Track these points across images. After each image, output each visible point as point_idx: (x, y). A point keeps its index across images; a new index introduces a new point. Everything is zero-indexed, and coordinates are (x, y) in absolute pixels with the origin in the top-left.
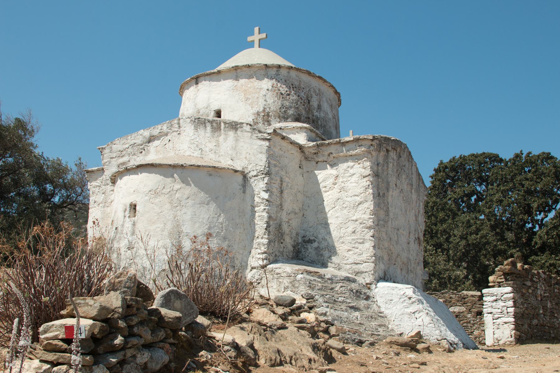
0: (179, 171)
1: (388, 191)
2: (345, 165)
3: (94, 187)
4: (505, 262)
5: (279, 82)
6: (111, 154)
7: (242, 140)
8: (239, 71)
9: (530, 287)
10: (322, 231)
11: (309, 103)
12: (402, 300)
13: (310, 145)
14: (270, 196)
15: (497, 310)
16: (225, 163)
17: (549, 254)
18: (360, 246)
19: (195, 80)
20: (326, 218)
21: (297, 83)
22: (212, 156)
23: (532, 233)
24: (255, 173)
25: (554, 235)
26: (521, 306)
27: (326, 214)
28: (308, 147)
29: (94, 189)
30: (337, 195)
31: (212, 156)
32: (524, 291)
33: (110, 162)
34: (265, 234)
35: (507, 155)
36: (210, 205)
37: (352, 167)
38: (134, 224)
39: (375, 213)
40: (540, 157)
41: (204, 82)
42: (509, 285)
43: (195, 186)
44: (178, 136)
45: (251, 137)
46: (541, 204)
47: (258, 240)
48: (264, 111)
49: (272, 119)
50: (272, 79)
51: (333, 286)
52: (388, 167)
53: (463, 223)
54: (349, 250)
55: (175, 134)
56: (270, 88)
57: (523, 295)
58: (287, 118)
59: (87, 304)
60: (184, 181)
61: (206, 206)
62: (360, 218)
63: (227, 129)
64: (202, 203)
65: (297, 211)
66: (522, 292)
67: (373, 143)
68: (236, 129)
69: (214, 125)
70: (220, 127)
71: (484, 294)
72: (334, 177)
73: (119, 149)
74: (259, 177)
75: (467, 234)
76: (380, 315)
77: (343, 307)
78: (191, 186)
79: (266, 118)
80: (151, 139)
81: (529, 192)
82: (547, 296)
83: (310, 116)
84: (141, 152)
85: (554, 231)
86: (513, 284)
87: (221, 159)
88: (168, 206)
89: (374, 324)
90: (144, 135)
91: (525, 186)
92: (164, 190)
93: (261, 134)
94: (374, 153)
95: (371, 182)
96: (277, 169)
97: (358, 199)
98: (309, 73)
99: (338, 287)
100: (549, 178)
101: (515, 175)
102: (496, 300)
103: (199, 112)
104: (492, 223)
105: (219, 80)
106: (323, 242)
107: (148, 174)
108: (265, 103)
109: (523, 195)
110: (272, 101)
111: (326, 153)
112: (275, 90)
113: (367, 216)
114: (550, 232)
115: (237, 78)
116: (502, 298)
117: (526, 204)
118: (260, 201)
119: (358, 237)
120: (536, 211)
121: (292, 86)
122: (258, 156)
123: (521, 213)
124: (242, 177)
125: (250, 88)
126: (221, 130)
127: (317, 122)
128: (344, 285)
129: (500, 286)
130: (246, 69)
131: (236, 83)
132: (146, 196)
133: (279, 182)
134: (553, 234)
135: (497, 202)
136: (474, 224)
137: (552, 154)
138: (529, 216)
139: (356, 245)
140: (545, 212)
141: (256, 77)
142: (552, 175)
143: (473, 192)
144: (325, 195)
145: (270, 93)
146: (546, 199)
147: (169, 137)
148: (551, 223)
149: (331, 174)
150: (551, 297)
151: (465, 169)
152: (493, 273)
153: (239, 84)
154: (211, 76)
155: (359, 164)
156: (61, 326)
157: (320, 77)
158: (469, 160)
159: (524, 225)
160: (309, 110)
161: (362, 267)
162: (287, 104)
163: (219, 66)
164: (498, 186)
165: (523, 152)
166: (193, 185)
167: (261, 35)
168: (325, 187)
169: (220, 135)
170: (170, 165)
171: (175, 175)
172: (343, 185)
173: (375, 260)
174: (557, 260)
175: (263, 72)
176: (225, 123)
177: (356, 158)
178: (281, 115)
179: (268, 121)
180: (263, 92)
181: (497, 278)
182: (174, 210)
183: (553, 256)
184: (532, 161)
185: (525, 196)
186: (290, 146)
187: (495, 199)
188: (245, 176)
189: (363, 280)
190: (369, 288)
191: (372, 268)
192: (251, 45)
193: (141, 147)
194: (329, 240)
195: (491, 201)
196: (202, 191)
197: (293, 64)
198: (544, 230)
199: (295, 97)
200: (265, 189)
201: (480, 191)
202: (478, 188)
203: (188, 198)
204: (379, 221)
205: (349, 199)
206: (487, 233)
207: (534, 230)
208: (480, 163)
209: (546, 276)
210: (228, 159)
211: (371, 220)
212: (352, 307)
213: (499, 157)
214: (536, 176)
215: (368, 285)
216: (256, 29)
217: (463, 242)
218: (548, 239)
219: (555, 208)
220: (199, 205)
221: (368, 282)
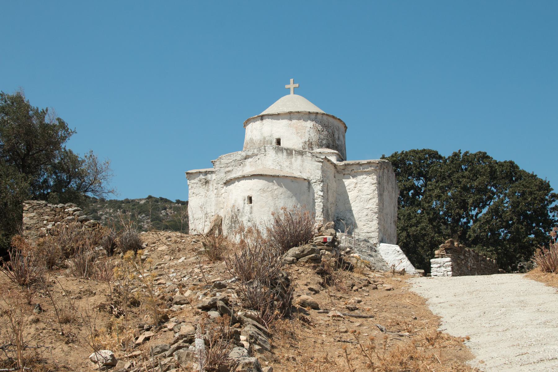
0: (276, 179)
1: (384, 192)
2: (361, 177)
3: (193, 184)
4: (446, 242)
5: (317, 123)
6: (220, 165)
7: (306, 161)
8: (292, 114)
9: (463, 260)
10: (348, 214)
11: (334, 136)
12: (394, 252)
13: (341, 165)
14: (323, 194)
15: (440, 273)
16: (297, 174)
17: (481, 246)
18: (371, 223)
19: (260, 117)
20: (350, 207)
21: (327, 124)
22: (288, 169)
23: (466, 227)
24: (315, 181)
25: (487, 228)
26: (457, 272)
27: (350, 204)
28: (340, 165)
29: (193, 185)
30: (357, 194)
31: (288, 169)
32: (459, 262)
33: (220, 170)
34: (321, 215)
35: (446, 153)
36: (293, 198)
37: (366, 178)
38: (251, 208)
39: (378, 205)
40: (477, 156)
41: (267, 119)
42: (449, 257)
43: (285, 187)
44: (264, 156)
45: (311, 160)
46: (476, 200)
47: (317, 218)
48: (309, 141)
49: (314, 147)
50: (313, 121)
51: (359, 243)
52: (384, 178)
53: (404, 216)
54: (364, 225)
55: (262, 155)
56: (312, 126)
57: (458, 264)
58: (322, 146)
59: (326, 232)
60: (279, 184)
61: (291, 199)
62: (371, 208)
63: (296, 155)
64: (289, 197)
65: (334, 202)
66: (457, 262)
67: (378, 165)
68: (302, 155)
69: (288, 151)
70: (292, 153)
71: (432, 262)
72: (354, 184)
73: (226, 162)
74: (317, 183)
75: (407, 226)
76: (382, 260)
77: (366, 254)
78: (283, 187)
79: (310, 145)
80: (247, 158)
81: (465, 189)
82: (475, 268)
83: (335, 144)
84: (240, 165)
85: (486, 225)
86: (452, 256)
87: (294, 172)
88: (271, 198)
89: (380, 264)
90: (242, 155)
91: (462, 183)
92: (268, 190)
93: (317, 159)
94: (378, 171)
95: (377, 187)
96: (325, 178)
97: (369, 197)
98: (333, 117)
99: (362, 244)
100: (485, 177)
101: (454, 172)
102: (440, 267)
103: (265, 139)
104: (431, 216)
105: (279, 120)
106: (349, 220)
107: (258, 180)
108: (309, 136)
109: (460, 191)
110: (314, 135)
111: (350, 170)
112: (315, 128)
113: (374, 206)
114: (483, 226)
115: (290, 119)
116: (444, 265)
117: (462, 200)
118: (318, 196)
119: (369, 218)
120: (471, 206)
121: (321, 123)
122: (316, 171)
123: (457, 208)
124: (308, 183)
125: (300, 126)
126: (292, 155)
127: (338, 148)
128: (364, 243)
129: (442, 257)
130: (297, 114)
131: (290, 122)
132: (258, 192)
133: (326, 186)
134: (485, 228)
135: (436, 197)
136: (415, 217)
137: (488, 154)
138: (465, 211)
139: (368, 222)
140: (479, 207)
141: (303, 119)
142: (487, 174)
143: (413, 187)
144: (349, 194)
145: (312, 130)
146: (480, 195)
147: (258, 157)
148: (484, 218)
149: (352, 182)
150: (478, 269)
151: (405, 164)
152: (437, 248)
153: (292, 123)
154: (273, 116)
155: (370, 176)
156: (322, 238)
157: (339, 119)
158: (410, 155)
159: (459, 220)
160: (334, 141)
161: (371, 235)
162: (322, 137)
164: (437, 182)
165: (461, 152)
166: (284, 187)
167: (295, 85)
168: (349, 189)
169: (292, 158)
170: (271, 175)
171: (274, 181)
172: (360, 188)
173: (379, 231)
174: (488, 251)
175: (307, 116)
176: (295, 151)
177: (368, 173)
178: (319, 144)
179: (312, 148)
180: (308, 129)
181: (441, 252)
182: (274, 200)
183: (485, 248)
184: (469, 159)
185: (462, 192)
186: (331, 165)
187: (434, 195)
188: (309, 182)
189: (374, 241)
190: (376, 246)
191: (377, 235)
192: (287, 92)
193: (240, 162)
194: (353, 219)
195: (430, 196)
196: (289, 190)
197: (324, 111)
198: (478, 224)
199: (326, 133)
200: (321, 190)
201: (418, 186)
202: (416, 183)
203: (281, 194)
204: (380, 209)
205: (364, 196)
206: (426, 226)
207: (469, 225)
208: (420, 159)
209: (475, 254)
210: (298, 172)
211: (377, 209)
212: (369, 255)
213: (438, 154)
214: (472, 174)
215: (375, 245)
216: (292, 80)
217: (404, 234)
218: (480, 233)
219: (489, 204)
220: (287, 198)
221: (375, 243)
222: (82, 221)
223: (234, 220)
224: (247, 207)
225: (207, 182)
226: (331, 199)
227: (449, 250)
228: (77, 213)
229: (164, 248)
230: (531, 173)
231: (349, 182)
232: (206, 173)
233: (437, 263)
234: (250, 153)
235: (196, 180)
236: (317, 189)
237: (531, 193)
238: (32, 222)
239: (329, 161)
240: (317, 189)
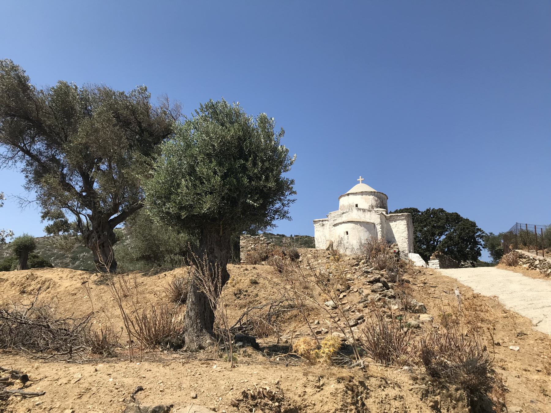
2: (399, 221)
22: (363, 218)
31: (363, 218)
57: (442, 263)
60: (361, 226)
79: (372, 207)
81: (434, 227)
97: (403, 231)
98: (382, 193)
115: (362, 195)
121: (377, 196)
137: (444, 209)
140: (439, 236)
144: (393, 230)
160: (383, 205)
163: (349, 189)
177: (402, 220)
180: (371, 199)
188: (374, 224)
192: (359, 182)
216: (360, 177)
222: (268, 244)
223: (340, 243)
224: (346, 236)
225: (323, 225)
226: (385, 233)
227: (437, 257)
228: (266, 240)
229: (310, 255)
230: (466, 218)
231: (392, 224)
232: (323, 221)
233: (432, 263)
234: (345, 211)
235: (318, 224)
236: (378, 227)
237: (468, 228)
238: (244, 244)
239: (383, 214)
240: (378, 227)
